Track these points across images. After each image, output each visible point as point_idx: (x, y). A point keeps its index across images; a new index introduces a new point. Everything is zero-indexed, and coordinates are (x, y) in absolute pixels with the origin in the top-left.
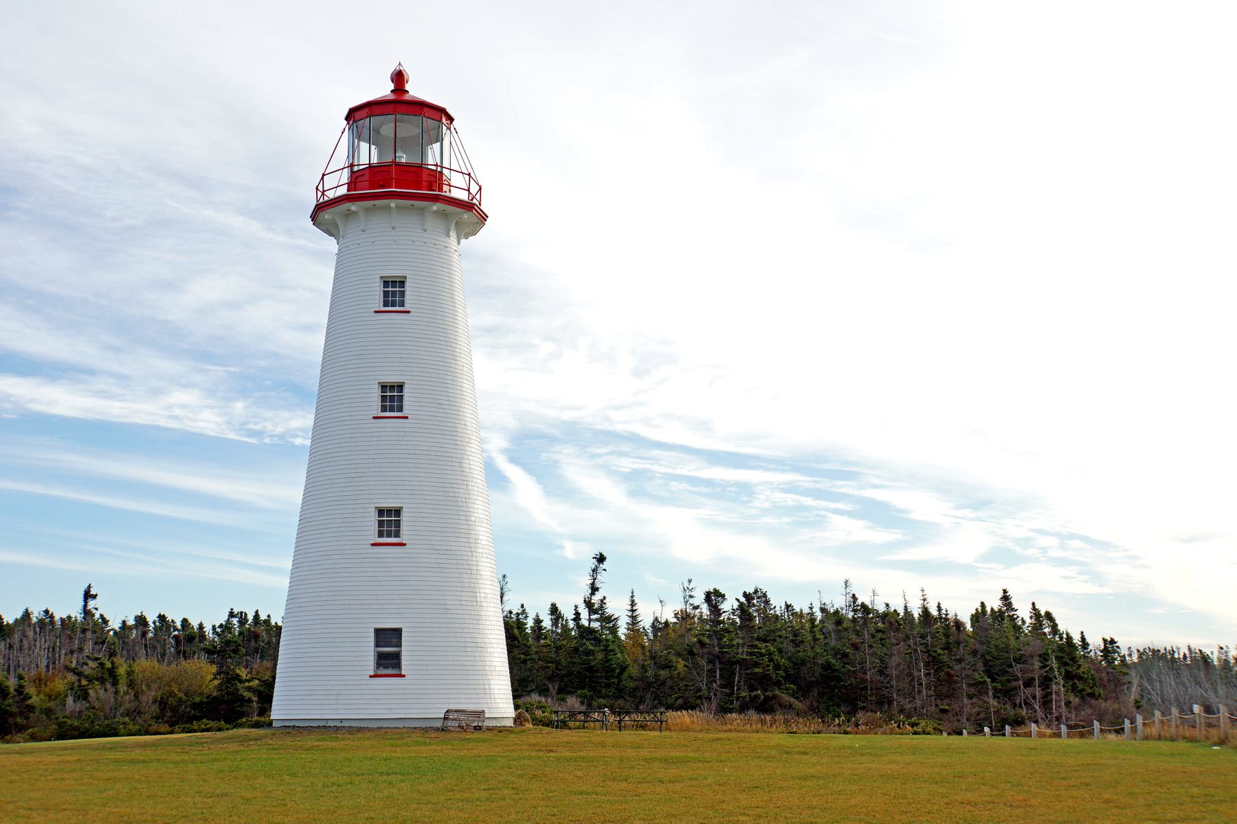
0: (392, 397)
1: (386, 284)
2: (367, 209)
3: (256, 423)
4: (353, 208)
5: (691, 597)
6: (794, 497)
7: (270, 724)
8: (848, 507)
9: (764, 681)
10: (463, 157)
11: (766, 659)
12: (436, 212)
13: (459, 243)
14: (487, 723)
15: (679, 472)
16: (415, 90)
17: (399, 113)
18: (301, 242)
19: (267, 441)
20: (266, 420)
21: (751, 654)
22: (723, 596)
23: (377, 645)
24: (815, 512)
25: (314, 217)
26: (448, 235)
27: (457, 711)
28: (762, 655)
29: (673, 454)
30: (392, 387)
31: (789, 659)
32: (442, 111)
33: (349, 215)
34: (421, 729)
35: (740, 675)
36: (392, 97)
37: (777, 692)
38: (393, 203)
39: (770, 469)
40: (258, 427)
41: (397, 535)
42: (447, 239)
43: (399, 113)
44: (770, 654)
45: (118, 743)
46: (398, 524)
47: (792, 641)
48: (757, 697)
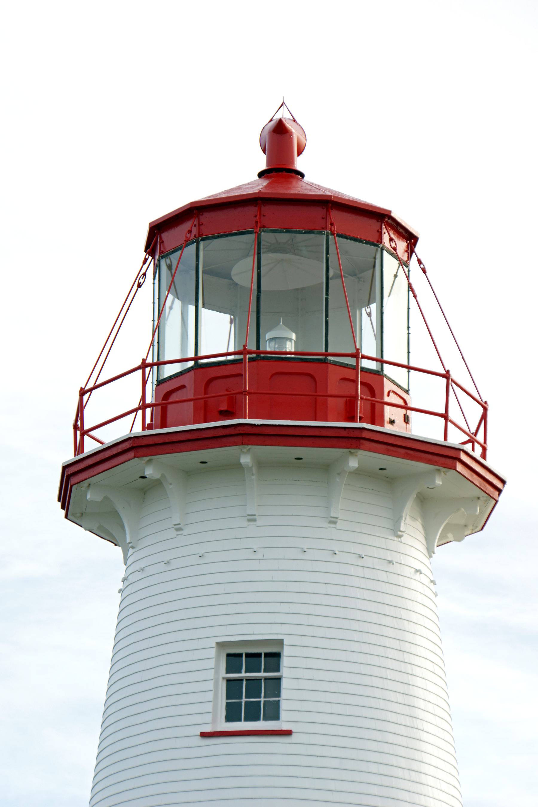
10: (436, 336)
12: (360, 473)
16: (320, 171)
17: (279, 232)
25: (65, 498)
26: (396, 532)
32: (382, 218)
33: (146, 491)
38: (247, 456)
42: (393, 543)
43: (279, 232)
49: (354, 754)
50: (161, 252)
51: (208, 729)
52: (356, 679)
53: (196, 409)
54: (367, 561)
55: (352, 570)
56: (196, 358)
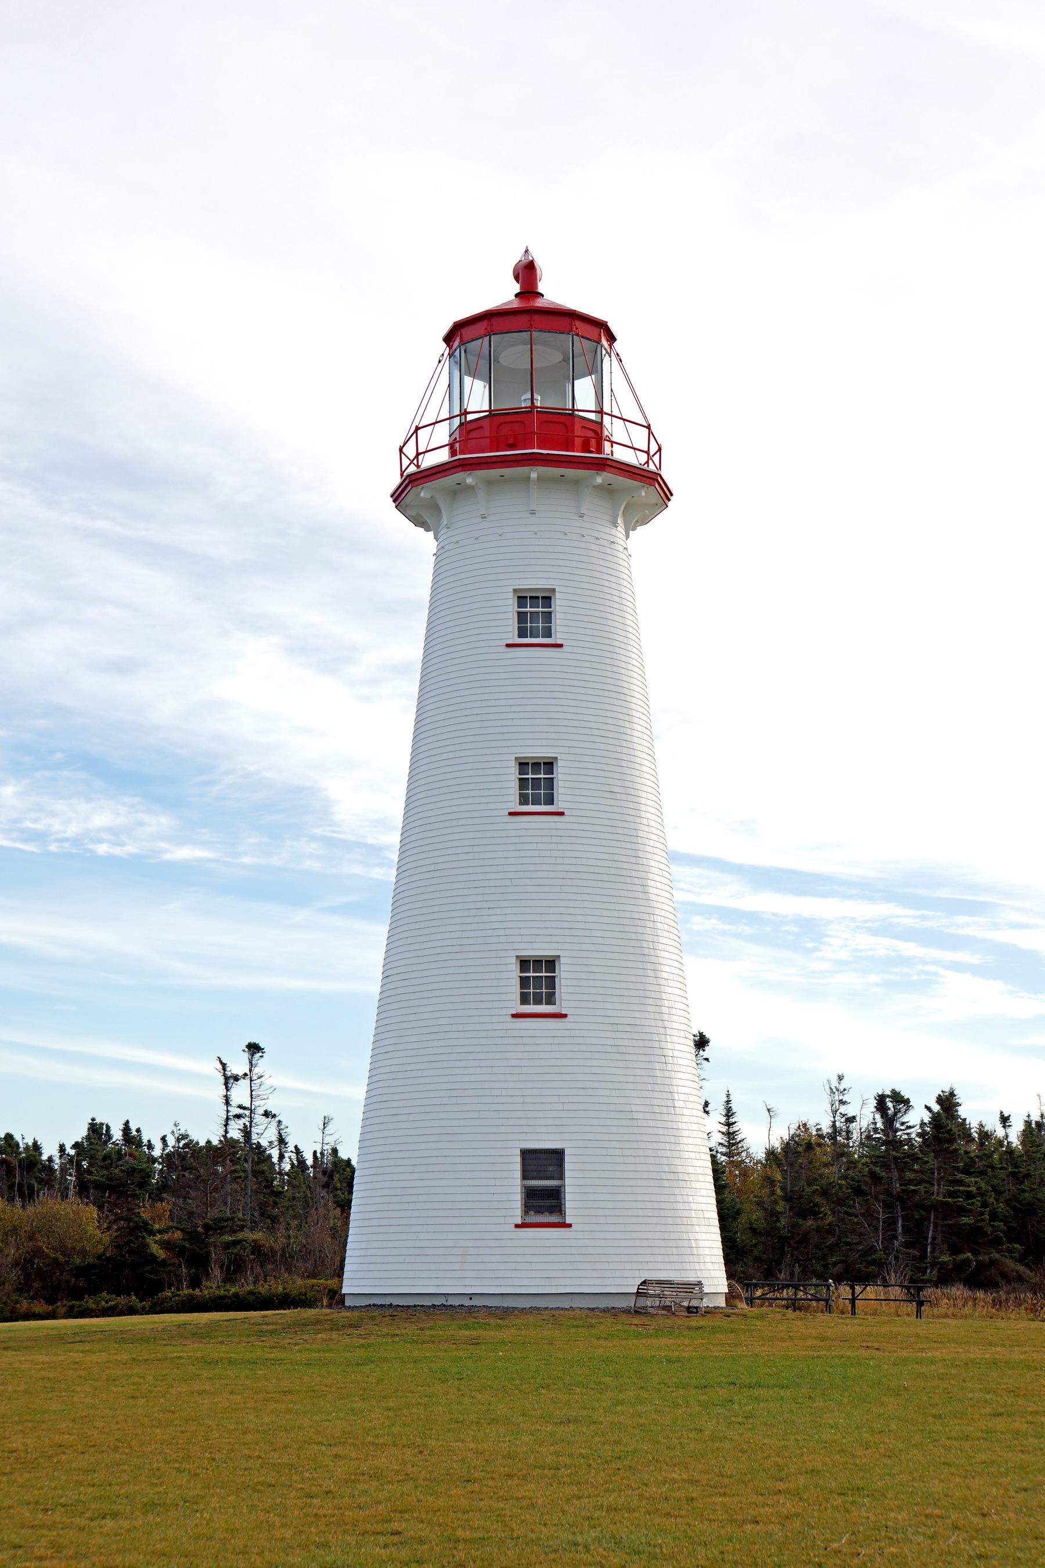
0: (537, 780)
1: (522, 600)
2: (489, 483)
3: (35, 821)
4: (469, 481)
5: (842, 1102)
6: (887, 941)
7: (336, 1298)
8: (975, 960)
9: (973, 1238)
10: (635, 397)
11: (977, 1201)
12: (599, 487)
13: (627, 537)
14: (706, 1303)
15: (704, 900)
16: (554, 291)
18: (102, 524)
19: (53, 848)
20: (53, 814)
21: (950, 1194)
22: (906, 1102)
23: (524, 1177)
24: (920, 967)
26: (615, 524)
27: (659, 1282)
28: (969, 1195)
29: (697, 871)
30: (536, 766)
31: (1007, 1202)
32: (602, 326)
33: (459, 492)
34: (606, 1310)
35: (936, 1226)
36: (516, 304)
37: (997, 1256)
38: (534, 472)
39: (850, 897)
40: (39, 826)
41: (550, 1000)
42: (613, 531)
44: (982, 1195)
45: (81, 1327)
46: (551, 982)
47: (1013, 1175)
48: (966, 1262)
49: (598, 659)
50: (461, 341)
51: (510, 642)
52: (597, 614)
53: (492, 442)
54: (601, 542)
55: (593, 547)
56: (490, 411)
